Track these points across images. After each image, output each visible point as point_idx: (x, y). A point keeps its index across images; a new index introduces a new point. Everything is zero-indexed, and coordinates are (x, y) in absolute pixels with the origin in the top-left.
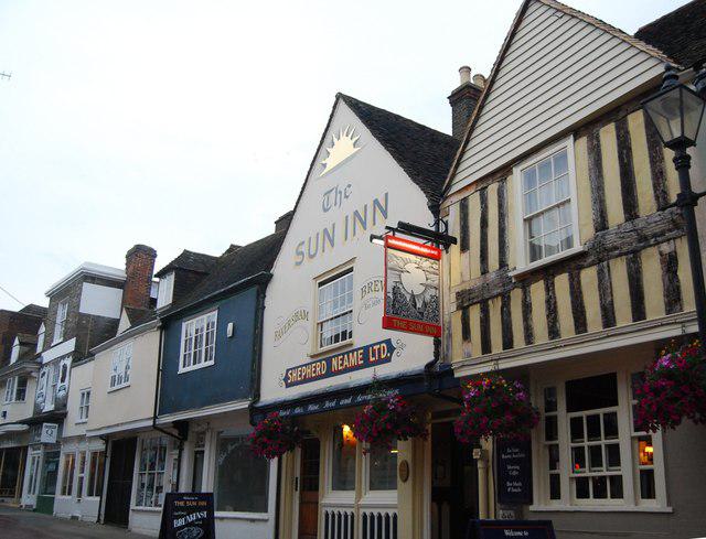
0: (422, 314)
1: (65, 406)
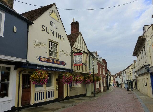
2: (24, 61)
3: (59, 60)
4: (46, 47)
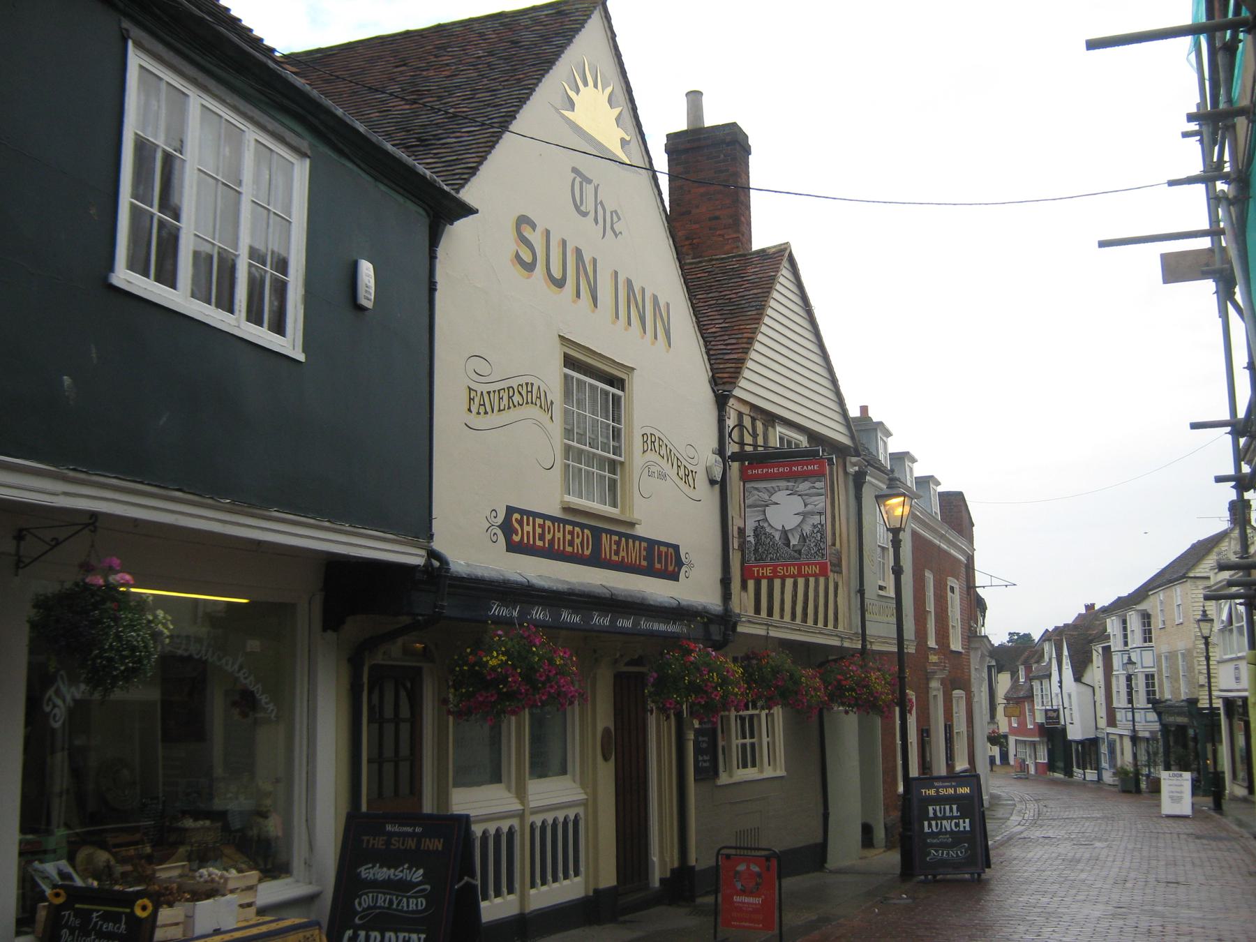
2: (415, 558)
3: (640, 531)
4: (544, 417)
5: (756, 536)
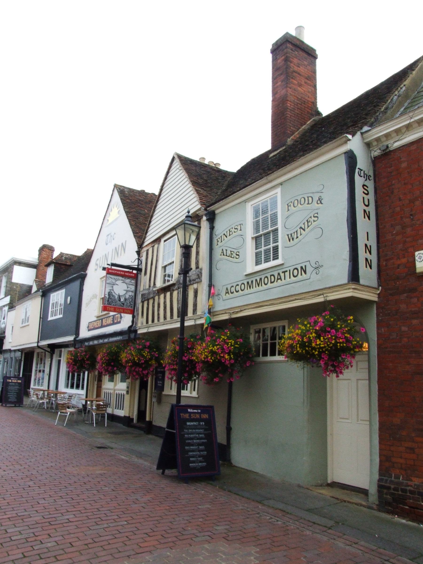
0: (124, 304)
1: (4, 332)
5: (109, 295)
